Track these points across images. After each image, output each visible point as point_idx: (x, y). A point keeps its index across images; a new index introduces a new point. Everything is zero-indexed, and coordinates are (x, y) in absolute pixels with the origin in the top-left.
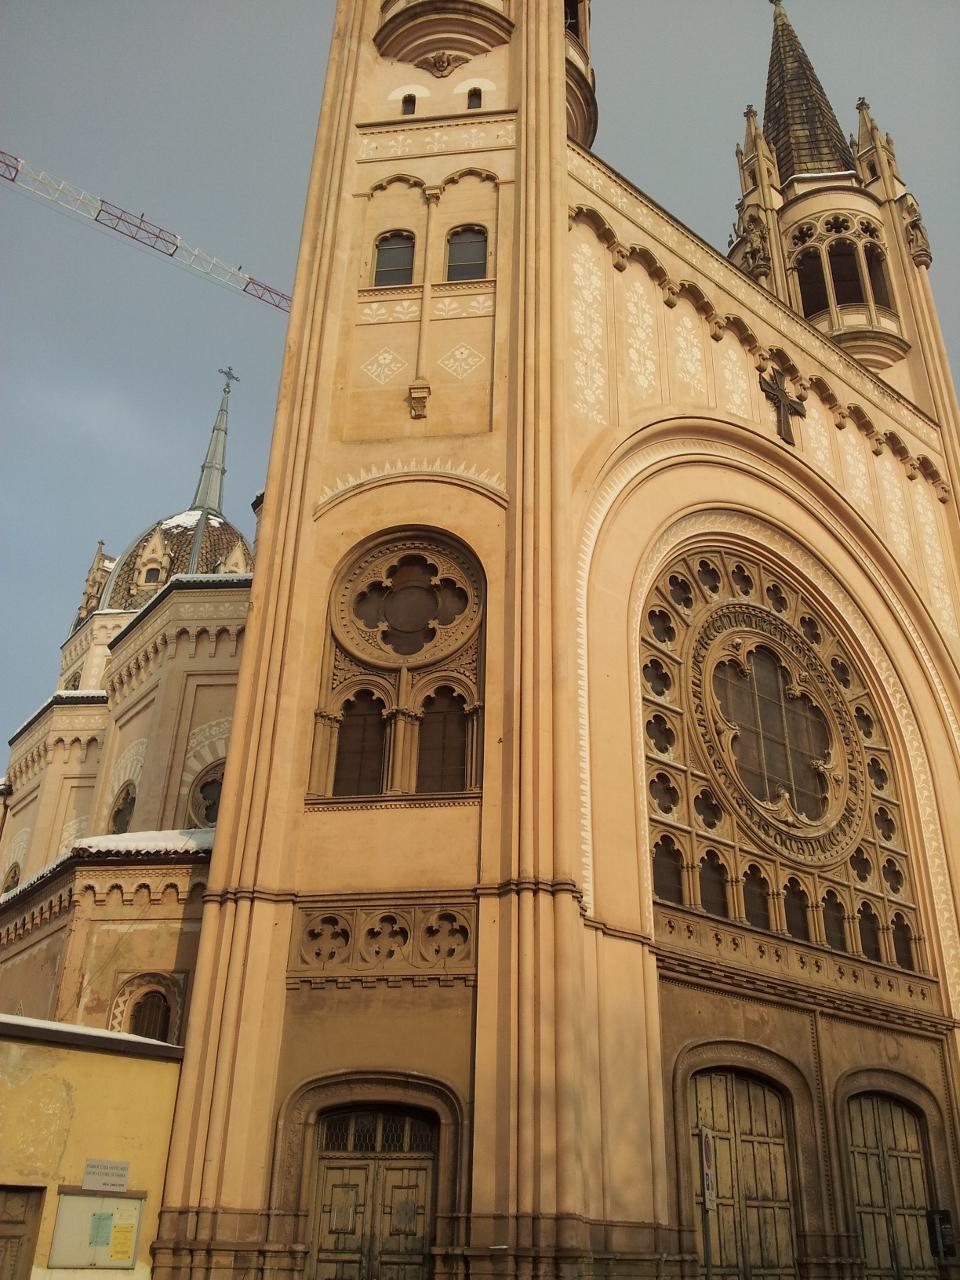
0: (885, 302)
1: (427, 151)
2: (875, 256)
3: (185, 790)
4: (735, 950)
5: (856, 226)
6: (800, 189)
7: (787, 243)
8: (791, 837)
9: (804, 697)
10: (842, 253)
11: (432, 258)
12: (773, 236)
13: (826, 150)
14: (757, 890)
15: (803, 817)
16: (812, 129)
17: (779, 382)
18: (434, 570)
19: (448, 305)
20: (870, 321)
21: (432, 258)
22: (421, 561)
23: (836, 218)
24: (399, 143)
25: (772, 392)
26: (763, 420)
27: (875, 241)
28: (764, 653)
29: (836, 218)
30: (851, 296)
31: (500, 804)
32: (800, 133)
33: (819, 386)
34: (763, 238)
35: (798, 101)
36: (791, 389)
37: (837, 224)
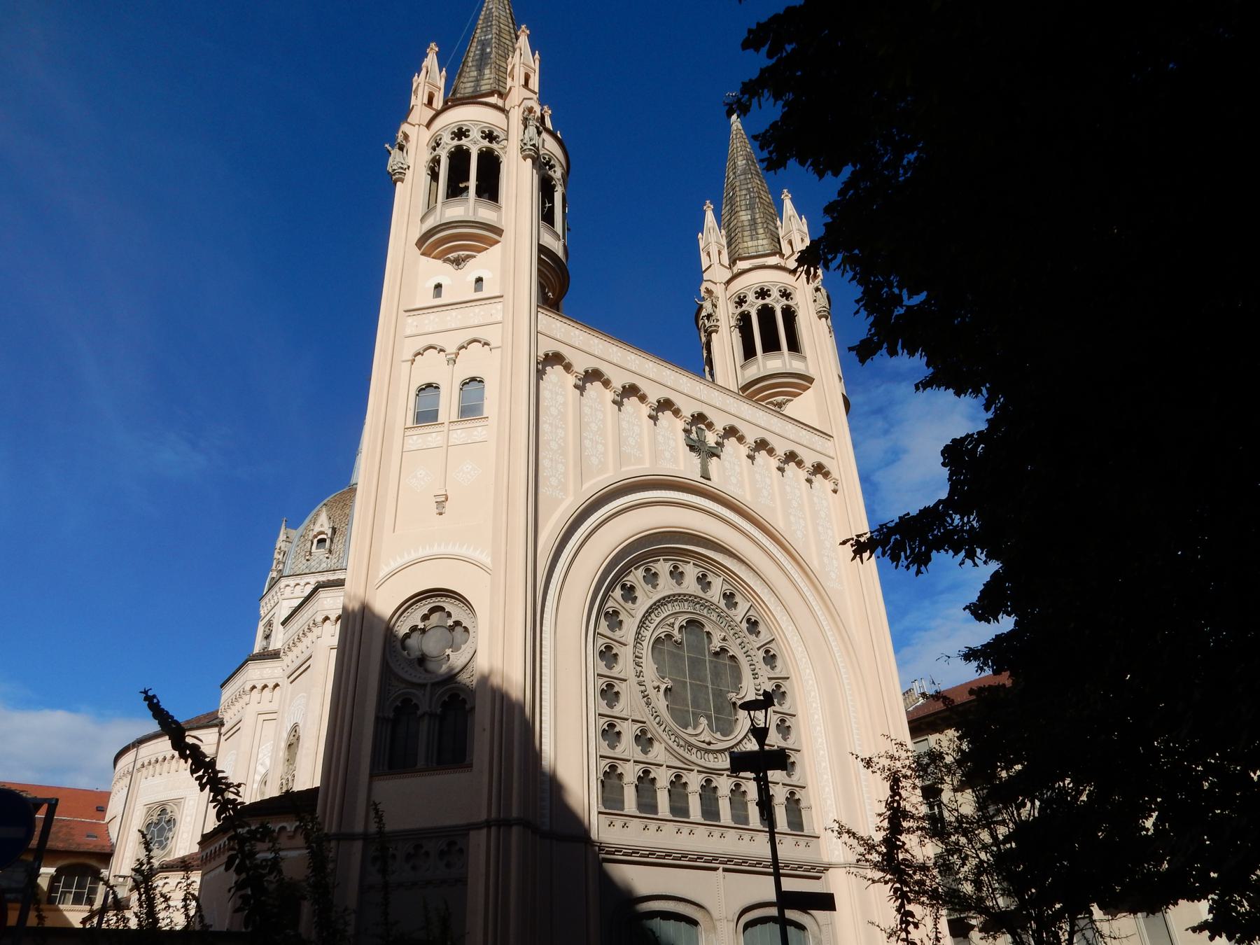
0: (794, 346)
1: (449, 327)
2: (789, 315)
3: (255, 786)
4: (146, 692)
5: (775, 293)
6: (742, 265)
7: (731, 307)
8: (707, 751)
9: (723, 650)
10: (766, 314)
11: (448, 404)
12: (720, 304)
13: (761, 231)
14: (794, 805)
15: (718, 735)
16: (753, 214)
17: (701, 437)
18: (449, 615)
19: (461, 434)
20: (784, 364)
21: (448, 404)
22: (441, 609)
23: (762, 289)
24: (431, 321)
25: (695, 447)
26: (686, 465)
27: (790, 303)
28: (693, 624)
29: (762, 289)
30: (771, 345)
31: (267, 797)
32: (744, 218)
33: (731, 432)
34: (715, 306)
35: (744, 192)
36: (711, 439)
37: (763, 293)
